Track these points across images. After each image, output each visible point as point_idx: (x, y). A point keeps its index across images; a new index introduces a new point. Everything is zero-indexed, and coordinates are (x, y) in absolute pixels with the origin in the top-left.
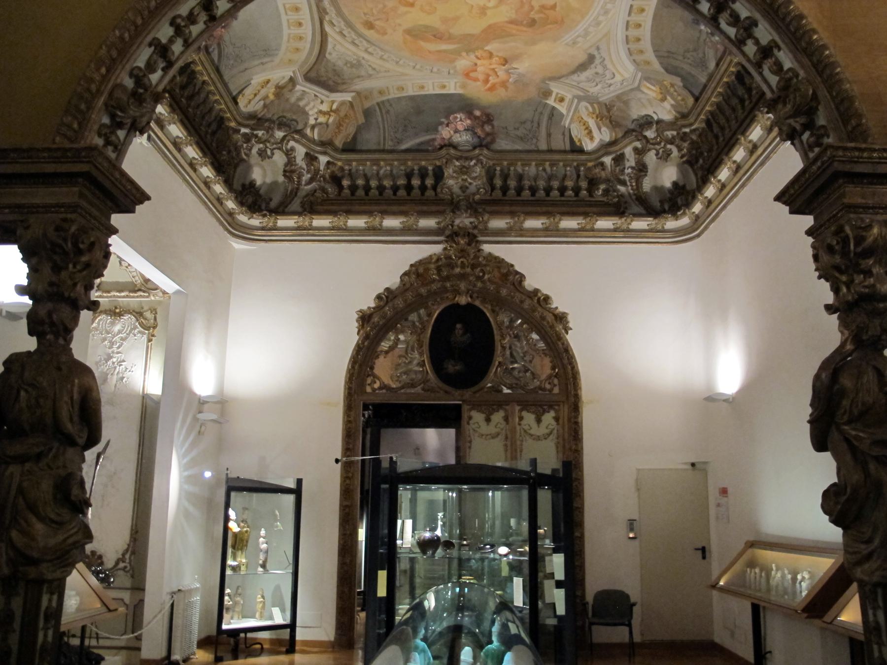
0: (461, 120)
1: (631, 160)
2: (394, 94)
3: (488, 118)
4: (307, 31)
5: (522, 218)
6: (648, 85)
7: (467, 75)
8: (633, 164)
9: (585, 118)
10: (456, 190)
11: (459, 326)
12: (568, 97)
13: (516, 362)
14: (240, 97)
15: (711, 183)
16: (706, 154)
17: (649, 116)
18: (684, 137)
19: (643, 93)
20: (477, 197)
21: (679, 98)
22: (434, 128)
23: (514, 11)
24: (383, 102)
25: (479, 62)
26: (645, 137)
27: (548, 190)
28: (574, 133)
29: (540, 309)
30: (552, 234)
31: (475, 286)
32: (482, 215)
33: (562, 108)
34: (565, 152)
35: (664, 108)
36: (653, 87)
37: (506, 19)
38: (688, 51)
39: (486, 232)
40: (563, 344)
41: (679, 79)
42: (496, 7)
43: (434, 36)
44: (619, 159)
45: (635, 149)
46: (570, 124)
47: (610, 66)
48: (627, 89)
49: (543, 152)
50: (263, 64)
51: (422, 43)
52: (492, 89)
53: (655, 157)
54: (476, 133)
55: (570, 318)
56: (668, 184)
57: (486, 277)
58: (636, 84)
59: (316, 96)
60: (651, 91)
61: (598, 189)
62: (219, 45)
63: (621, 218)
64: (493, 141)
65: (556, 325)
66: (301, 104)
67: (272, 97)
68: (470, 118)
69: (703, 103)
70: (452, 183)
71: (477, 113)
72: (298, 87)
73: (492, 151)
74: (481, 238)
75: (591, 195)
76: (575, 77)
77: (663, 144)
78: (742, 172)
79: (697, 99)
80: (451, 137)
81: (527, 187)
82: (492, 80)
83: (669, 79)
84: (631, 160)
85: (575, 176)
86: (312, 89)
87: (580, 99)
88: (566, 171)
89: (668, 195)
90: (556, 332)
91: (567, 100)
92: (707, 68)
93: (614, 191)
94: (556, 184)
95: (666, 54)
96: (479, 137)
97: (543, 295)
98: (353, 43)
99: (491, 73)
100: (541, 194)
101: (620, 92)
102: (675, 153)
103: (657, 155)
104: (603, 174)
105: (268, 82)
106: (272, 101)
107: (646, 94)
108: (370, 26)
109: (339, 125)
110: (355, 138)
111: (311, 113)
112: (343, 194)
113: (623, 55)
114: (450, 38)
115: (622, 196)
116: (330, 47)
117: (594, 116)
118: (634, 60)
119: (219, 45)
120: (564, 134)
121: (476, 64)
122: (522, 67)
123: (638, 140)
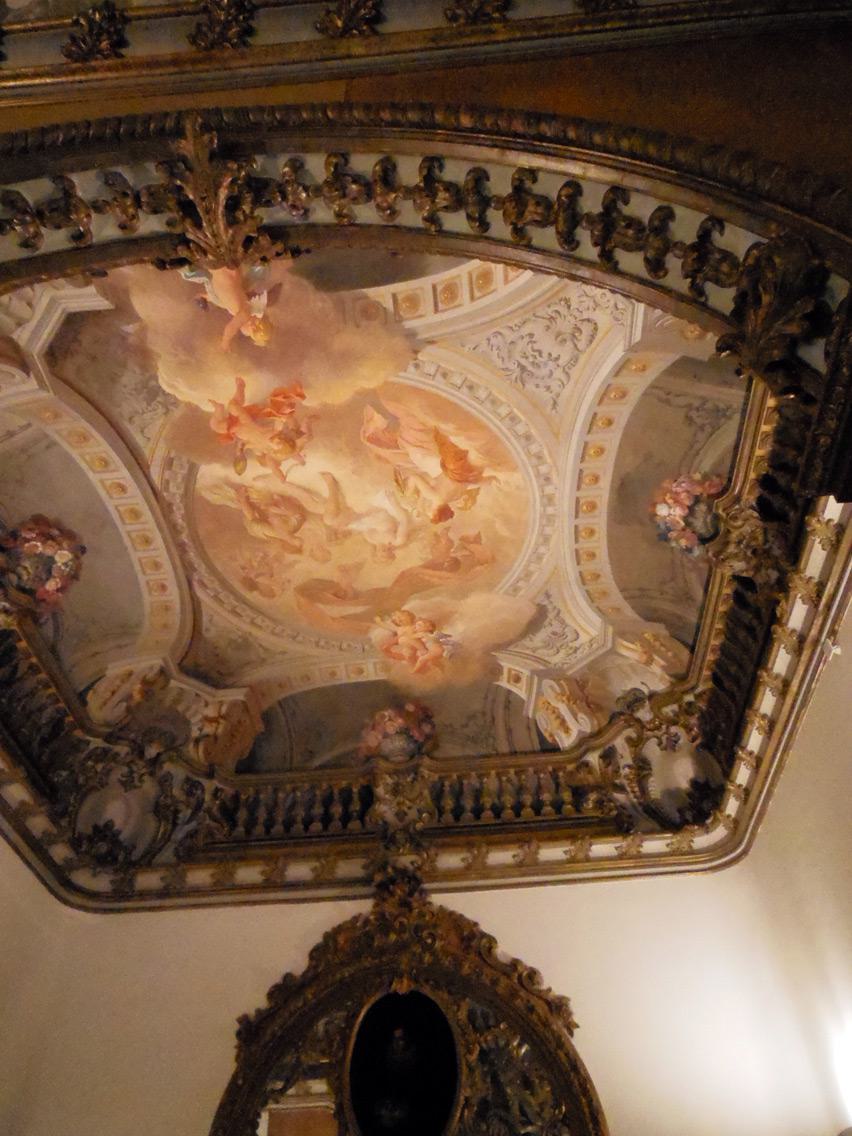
0: (390, 720)
1: (625, 756)
2: (301, 687)
3: (425, 715)
4: (173, 595)
5: (484, 850)
6: (625, 643)
7: (387, 651)
8: (629, 761)
9: (554, 703)
10: (390, 817)
11: (398, 1033)
12: (525, 673)
13: (531, 1123)
14: (91, 692)
15: (742, 759)
16: (723, 725)
17: (636, 689)
18: (688, 710)
19: (622, 656)
20: (419, 826)
21: (670, 654)
22: (355, 734)
23: (428, 550)
24: (285, 699)
25: (400, 630)
26: (638, 721)
27: (518, 808)
28: (543, 726)
29: (522, 993)
30: (530, 872)
31: (421, 961)
32: (426, 850)
33: (520, 691)
34: (533, 752)
35: (653, 673)
36: (631, 646)
37: (421, 563)
38: (663, 583)
39: (435, 875)
40: (567, 1055)
41: (662, 626)
42: (404, 545)
43: (335, 595)
44: (609, 756)
45: (629, 740)
46: (535, 711)
47: (569, 621)
48: (601, 652)
49: (504, 755)
50: (120, 647)
51: (321, 606)
52: (423, 669)
53: (657, 749)
54: (412, 737)
55: (574, 1006)
56: (684, 785)
57: (438, 944)
58: (609, 645)
59: (197, 695)
60: (631, 652)
61: (587, 800)
62: (54, 615)
63: (625, 837)
64: (436, 746)
65: (551, 1019)
66: (180, 708)
67: (137, 697)
68: (401, 716)
69: (702, 650)
70: (385, 809)
71: (410, 708)
72: (173, 683)
73: (436, 759)
74: (426, 886)
75: (578, 809)
76: (527, 642)
77: (664, 727)
78: (779, 727)
79: (692, 650)
80: (380, 744)
81: (488, 805)
82: (422, 657)
83: (651, 631)
84: (625, 756)
85: (553, 786)
86: (190, 685)
87: (542, 675)
88: (539, 778)
89: (688, 800)
90: (553, 1032)
91: (524, 680)
92: (693, 600)
93: (610, 801)
94: (528, 799)
95: (637, 593)
96: (416, 741)
97: (526, 968)
98: (234, 612)
99: (417, 645)
100: (508, 814)
101: (591, 658)
102: (684, 738)
103: (660, 744)
104: (591, 779)
105: (130, 674)
106: (139, 705)
107: (627, 658)
108: (252, 586)
109: (232, 734)
110: (253, 754)
111: (193, 721)
112: (235, 833)
113: (583, 603)
114: (356, 597)
115: (623, 807)
116: (205, 619)
117: (564, 698)
118: (597, 607)
119: (54, 615)
120: (529, 728)
121: (395, 634)
122: (457, 631)
123: (630, 726)
